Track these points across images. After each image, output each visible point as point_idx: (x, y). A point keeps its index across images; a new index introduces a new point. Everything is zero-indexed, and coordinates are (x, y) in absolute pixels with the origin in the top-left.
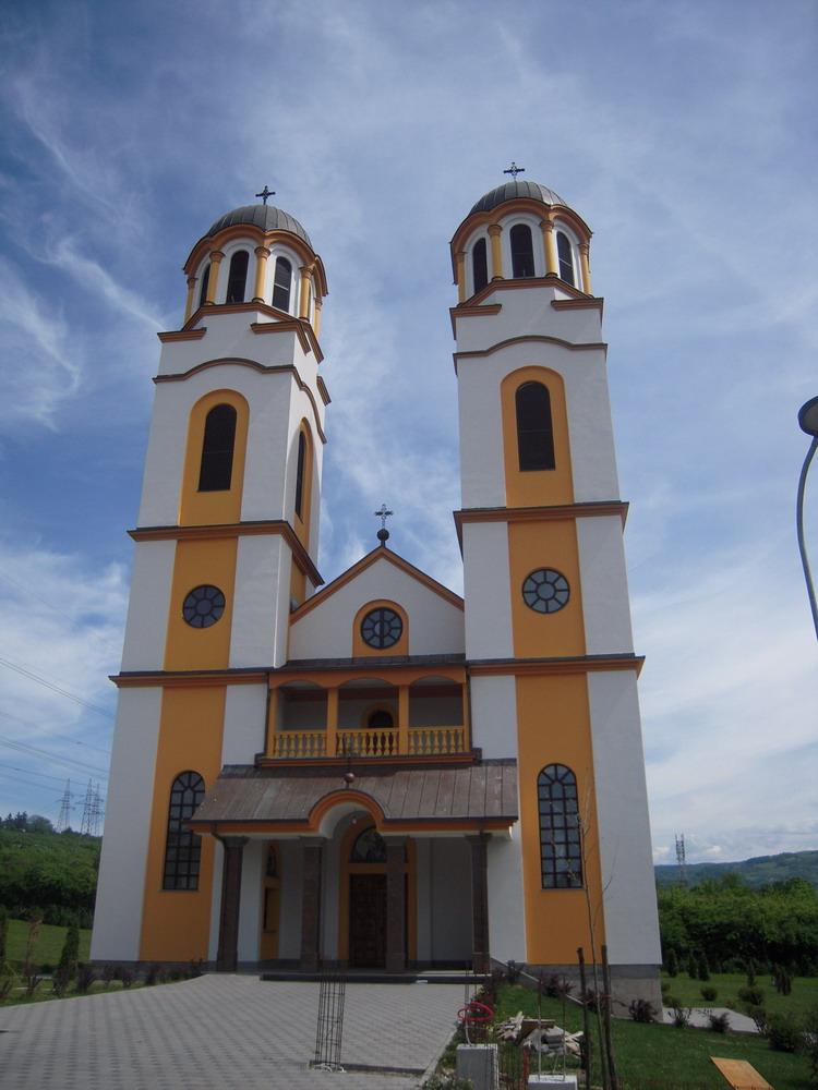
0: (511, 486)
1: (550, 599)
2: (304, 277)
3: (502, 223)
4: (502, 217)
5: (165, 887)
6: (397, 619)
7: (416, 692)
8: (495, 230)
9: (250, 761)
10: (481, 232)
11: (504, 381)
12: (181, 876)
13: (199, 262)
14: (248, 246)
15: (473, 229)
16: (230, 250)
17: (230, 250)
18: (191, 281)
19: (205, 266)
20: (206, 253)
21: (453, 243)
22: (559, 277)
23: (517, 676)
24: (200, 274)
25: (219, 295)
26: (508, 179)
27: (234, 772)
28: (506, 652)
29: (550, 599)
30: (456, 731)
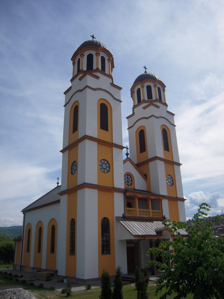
0: (98, 132)
1: (106, 168)
2: (109, 62)
3: (84, 54)
4: (84, 52)
5: (102, 254)
6: (107, 172)
7: (140, 199)
8: (82, 55)
9: (121, 216)
10: (79, 57)
11: (99, 100)
12: (105, 250)
13: (76, 58)
14: (93, 53)
15: (77, 55)
16: (86, 54)
17: (86, 54)
18: (74, 63)
19: (78, 59)
20: (79, 54)
21: (72, 59)
22: (100, 69)
23: (98, 190)
24: (76, 61)
25: (84, 67)
26: (91, 39)
27: (118, 219)
28: (95, 182)
29: (106, 168)
30: (133, 210)
